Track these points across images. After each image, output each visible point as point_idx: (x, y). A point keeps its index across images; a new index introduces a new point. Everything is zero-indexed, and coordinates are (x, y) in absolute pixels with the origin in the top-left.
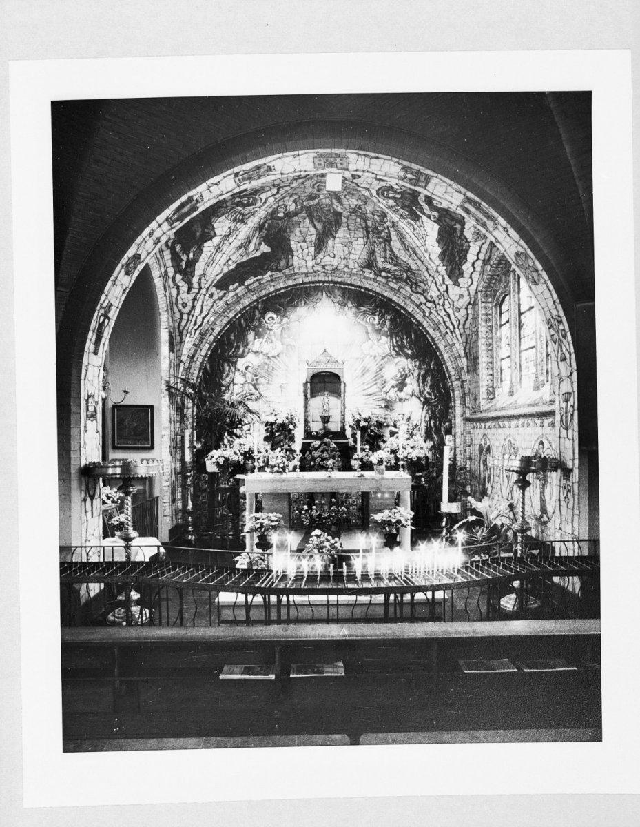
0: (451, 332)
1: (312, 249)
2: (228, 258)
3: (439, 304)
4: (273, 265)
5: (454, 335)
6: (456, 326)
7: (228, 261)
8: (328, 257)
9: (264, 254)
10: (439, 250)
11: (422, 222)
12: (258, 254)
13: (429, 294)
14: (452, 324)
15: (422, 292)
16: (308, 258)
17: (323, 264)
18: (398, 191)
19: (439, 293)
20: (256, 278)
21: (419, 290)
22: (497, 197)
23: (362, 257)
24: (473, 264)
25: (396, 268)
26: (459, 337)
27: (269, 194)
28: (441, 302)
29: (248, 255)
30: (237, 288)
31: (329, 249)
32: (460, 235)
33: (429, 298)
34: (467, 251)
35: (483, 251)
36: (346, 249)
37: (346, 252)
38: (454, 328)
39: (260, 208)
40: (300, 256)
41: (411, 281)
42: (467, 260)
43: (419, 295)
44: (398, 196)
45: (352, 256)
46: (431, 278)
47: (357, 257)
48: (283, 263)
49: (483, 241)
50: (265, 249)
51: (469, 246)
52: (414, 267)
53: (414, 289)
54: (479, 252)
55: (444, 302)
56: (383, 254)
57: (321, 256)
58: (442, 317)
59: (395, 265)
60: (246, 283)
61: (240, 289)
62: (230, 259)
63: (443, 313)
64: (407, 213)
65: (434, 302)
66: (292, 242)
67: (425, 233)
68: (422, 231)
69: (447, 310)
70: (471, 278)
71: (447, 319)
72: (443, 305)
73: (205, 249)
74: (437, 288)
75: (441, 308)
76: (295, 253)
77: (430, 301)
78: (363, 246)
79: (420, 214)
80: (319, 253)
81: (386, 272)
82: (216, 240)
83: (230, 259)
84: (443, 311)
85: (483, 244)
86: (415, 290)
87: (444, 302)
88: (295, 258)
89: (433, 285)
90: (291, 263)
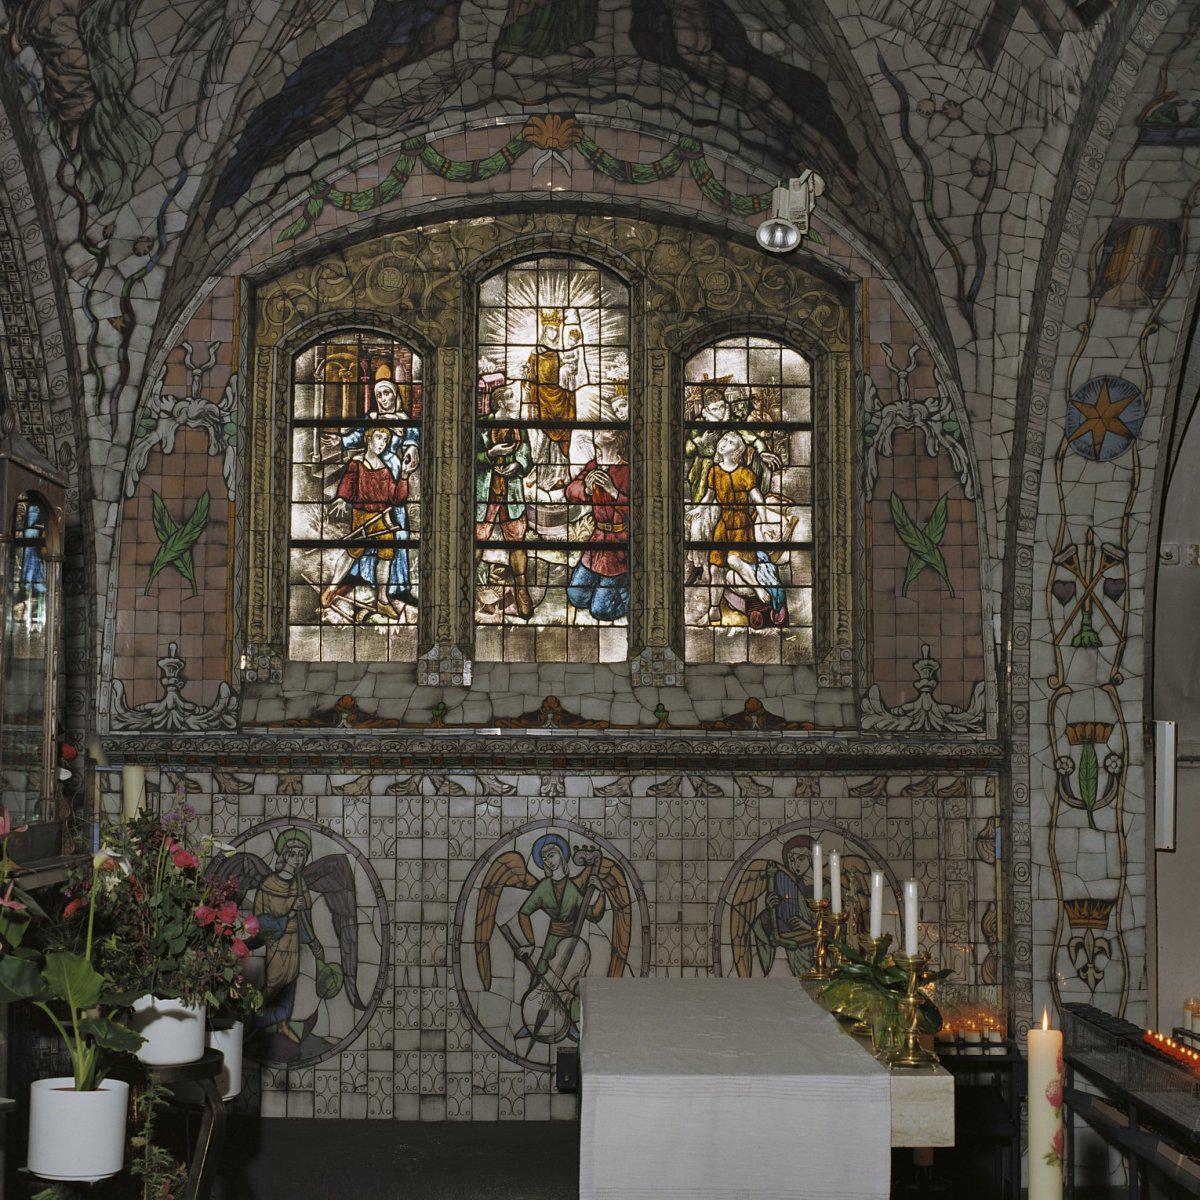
0: (100, 391)
3: (115, 268)
5: (106, 407)
6: (135, 374)
13: (106, 220)
14: (125, 364)
15: (88, 197)
19: (152, 231)
21: (85, 187)
22: (624, 45)
25: (83, 60)
26: (124, 420)
28: (134, 264)
33: (95, 232)
34: (311, 133)
38: (123, 380)
42: (284, 160)
43: (72, 201)
46: (174, 167)
52: (145, 95)
53: (69, 170)
58: (95, 321)
59: (90, 48)
63: (107, 310)
65: (102, 256)
69: (137, 305)
71: (111, 336)
72: (132, 281)
74: (163, 211)
75: (117, 286)
77: (88, 244)
81: (40, 55)
86: (69, 180)
89: (158, 194)
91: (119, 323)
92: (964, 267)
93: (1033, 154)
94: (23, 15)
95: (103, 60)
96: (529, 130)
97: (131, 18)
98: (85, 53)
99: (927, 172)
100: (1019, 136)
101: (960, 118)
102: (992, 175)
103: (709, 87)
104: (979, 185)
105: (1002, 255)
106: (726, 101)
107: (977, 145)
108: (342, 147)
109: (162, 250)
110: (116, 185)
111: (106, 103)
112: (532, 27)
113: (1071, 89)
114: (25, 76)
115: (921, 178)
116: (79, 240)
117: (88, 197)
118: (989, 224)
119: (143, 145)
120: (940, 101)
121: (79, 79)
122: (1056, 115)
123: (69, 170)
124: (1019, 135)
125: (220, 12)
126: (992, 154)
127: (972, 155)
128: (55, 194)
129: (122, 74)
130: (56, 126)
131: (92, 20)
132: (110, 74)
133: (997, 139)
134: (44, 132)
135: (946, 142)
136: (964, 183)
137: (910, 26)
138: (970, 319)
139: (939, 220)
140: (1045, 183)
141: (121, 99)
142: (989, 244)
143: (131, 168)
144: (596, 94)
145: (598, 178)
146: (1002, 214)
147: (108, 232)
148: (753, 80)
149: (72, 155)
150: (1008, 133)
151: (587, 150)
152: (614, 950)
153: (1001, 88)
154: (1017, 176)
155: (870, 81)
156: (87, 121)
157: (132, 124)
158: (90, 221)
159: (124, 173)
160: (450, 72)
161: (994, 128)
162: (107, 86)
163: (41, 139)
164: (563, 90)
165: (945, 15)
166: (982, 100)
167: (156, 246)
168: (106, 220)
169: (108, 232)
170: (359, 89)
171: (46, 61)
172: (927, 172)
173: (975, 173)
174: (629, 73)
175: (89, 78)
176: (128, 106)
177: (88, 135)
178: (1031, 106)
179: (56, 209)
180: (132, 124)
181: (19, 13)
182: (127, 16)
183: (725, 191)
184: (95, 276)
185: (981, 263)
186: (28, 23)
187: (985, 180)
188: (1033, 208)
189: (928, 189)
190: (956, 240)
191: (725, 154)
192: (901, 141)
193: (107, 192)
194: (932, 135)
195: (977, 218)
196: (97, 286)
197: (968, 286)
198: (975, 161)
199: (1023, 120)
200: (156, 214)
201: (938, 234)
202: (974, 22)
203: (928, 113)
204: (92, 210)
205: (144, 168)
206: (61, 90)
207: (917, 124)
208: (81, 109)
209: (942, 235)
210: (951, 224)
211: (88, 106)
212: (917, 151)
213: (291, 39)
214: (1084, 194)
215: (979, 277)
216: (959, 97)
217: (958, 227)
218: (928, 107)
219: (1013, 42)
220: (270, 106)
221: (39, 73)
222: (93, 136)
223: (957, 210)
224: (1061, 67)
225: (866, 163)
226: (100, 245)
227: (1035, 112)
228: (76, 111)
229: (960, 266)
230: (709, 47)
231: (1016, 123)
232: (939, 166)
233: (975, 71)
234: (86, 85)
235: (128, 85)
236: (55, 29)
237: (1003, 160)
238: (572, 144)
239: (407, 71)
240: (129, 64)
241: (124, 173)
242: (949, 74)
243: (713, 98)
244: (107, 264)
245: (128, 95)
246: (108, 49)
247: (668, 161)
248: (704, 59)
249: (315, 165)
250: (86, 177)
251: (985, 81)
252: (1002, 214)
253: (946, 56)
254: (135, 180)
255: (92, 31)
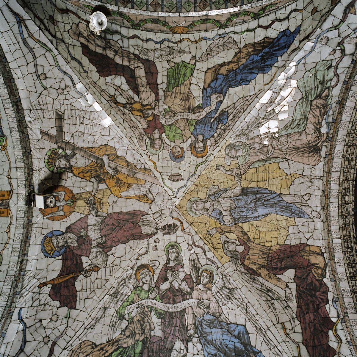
1: (298, 221)
2: (279, 326)
3: (339, 36)
4: (316, 273)
7: (284, 328)
8: (309, 202)
9: (296, 278)
10: (260, 75)
11: (228, 107)
12: (293, 286)
13: (332, 57)
16: (312, 227)
17: (319, 209)
18: (193, 139)
20: (330, 302)
22: (158, 65)
23: (306, 160)
24: (267, 28)
27: (202, 256)
29: (287, 299)
30: (337, 336)
31: (298, 201)
32: (235, 62)
33: (338, 54)
34: (254, 45)
35: (245, 27)
36: (297, 181)
37: (302, 180)
39: (218, 268)
40: (308, 236)
41: (322, 91)
42: (265, 38)
43: (339, 71)
44: (200, 138)
45: (307, 173)
47: (306, 167)
48: (314, 259)
49: (232, 35)
50: (291, 273)
51: (246, 46)
54: (248, 30)
55: (329, 30)
56: (296, 137)
57: (308, 211)
59: (306, 118)
60: (334, 320)
61: (341, 333)
62: (283, 324)
64: (220, 125)
66: (288, 242)
67: (241, 100)
68: (239, 104)
69: (340, 16)
70: (287, 18)
72: (336, 27)
73: (258, 348)
75: (343, 27)
76: (304, 241)
77: (343, 51)
78: (290, 162)
79: (219, 112)
80: (304, 213)
81: (320, 127)
82: (250, 328)
83: (283, 324)
84: (348, 21)
85: (235, 33)
86: (335, 79)
87: (329, 30)
88: (310, 242)
89: (309, 59)
90: (318, 250)
91: (352, 10)
92: (29, 36)
93: (30, 91)
94: (318, 143)
95: (304, 112)
96: (187, 30)
97: (291, 121)
98: (308, 118)
99: (59, 67)
100: (37, 95)
101: (57, 90)
102: (38, 77)
103: (134, 54)
104: (40, 71)
105: (19, 48)
106: (127, 50)
107: (48, 83)
108: (246, 33)
109: (318, 37)
110: (321, 69)
111: (310, 99)
112: (185, 75)
113: (30, 122)
114: (328, 124)
115: (60, 64)
116: (345, 55)
117: (332, 69)
118: (30, 57)
119: (305, 79)
120: (65, 93)
121: (314, 111)
122: (30, 110)
123: (333, 83)
124: (38, 95)
125: (267, 114)
126: (42, 83)
127: (48, 79)
128: (342, 78)
129: (301, 105)
130: (328, 101)
131: (301, 126)
132: (304, 107)
133: (43, 89)
134: (333, 102)
135: (58, 80)
136: (46, 68)
137: (82, 112)
138: (15, 14)
139: (47, 50)
140: (19, 84)
141: (305, 97)
142: (26, 50)
143: (313, 73)
144: (166, 43)
145: (164, 20)
146: (28, 64)
147: (333, 52)
148: (121, 63)
149: (328, 88)
150: (41, 94)
151: (168, 26)
152: (316, 77)
153: (50, 107)
154: (30, 79)
155: (88, 92)
156: (319, 96)
157: (305, 87)
158: (337, 60)
159: (316, 72)
160: (209, 57)
161: (45, 92)
162: (307, 104)
163: (335, 100)
164: (176, 45)
165: (74, 120)
166: (53, 99)
167: (319, 39)
168: (332, 57)
169: (333, 52)
170: (236, 58)
171: (319, 123)
172: (59, 67)
173: (44, 74)
174: (157, 54)
175: (311, 109)
176: (304, 95)
177: (320, 92)
178: (39, 108)
179: (346, 72)
180: (305, 87)
181: (319, 145)
182: (292, 122)
183: (122, 17)
184: (349, 36)
185: (24, 40)
186: (318, 140)
187: (40, 73)
188: (18, 71)
189: (56, 61)
190: (37, 45)
191: (124, 25)
192: (71, 75)
193: (326, 68)
194: (63, 80)
195: (35, 58)
196: (350, 31)
197: (23, 27)
198: (46, 78)
199: (39, 101)
200: (313, 52)
201: (44, 44)
202: (66, 122)
203: (67, 87)
204: (334, 64)
205: (309, 71)
206: (320, 111)
207: (69, 83)
208: (318, 101)
209: (43, 45)
210: (43, 51)
211: (315, 101)
212: (65, 73)
213: (251, 96)
214: (6, 103)
215: (22, 34)
216: (61, 97)
217: (39, 51)
218: (68, 89)
219: (53, 123)
220: (263, 70)
221: (324, 121)
222: (319, 90)
223: (43, 56)
224: (37, 127)
225: (78, 52)
226: (339, 48)
227: (36, 107)
228: (320, 101)
229: (31, 35)
230: (135, 70)
231: (40, 99)
232: (56, 71)
233: (59, 107)
234: (313, 108)
235: (301, 100)
236: (312, 132)
237: (37, 82)
238: (173, 27)
239: (221, 61)
240: (298, 107)
241: (316, 72)
242: (66, 102)
243: (132, 50)
244: (341, 39)
245: (303, 97)
246: (301, 115)
247: (142, 24)
248: (136, 65)
249: (256, 28)
250: (329, 78)
251: (55, 106)
252: (28, 64)
253: (69, 107)
254: (315, 67)
255: (303, 124)
